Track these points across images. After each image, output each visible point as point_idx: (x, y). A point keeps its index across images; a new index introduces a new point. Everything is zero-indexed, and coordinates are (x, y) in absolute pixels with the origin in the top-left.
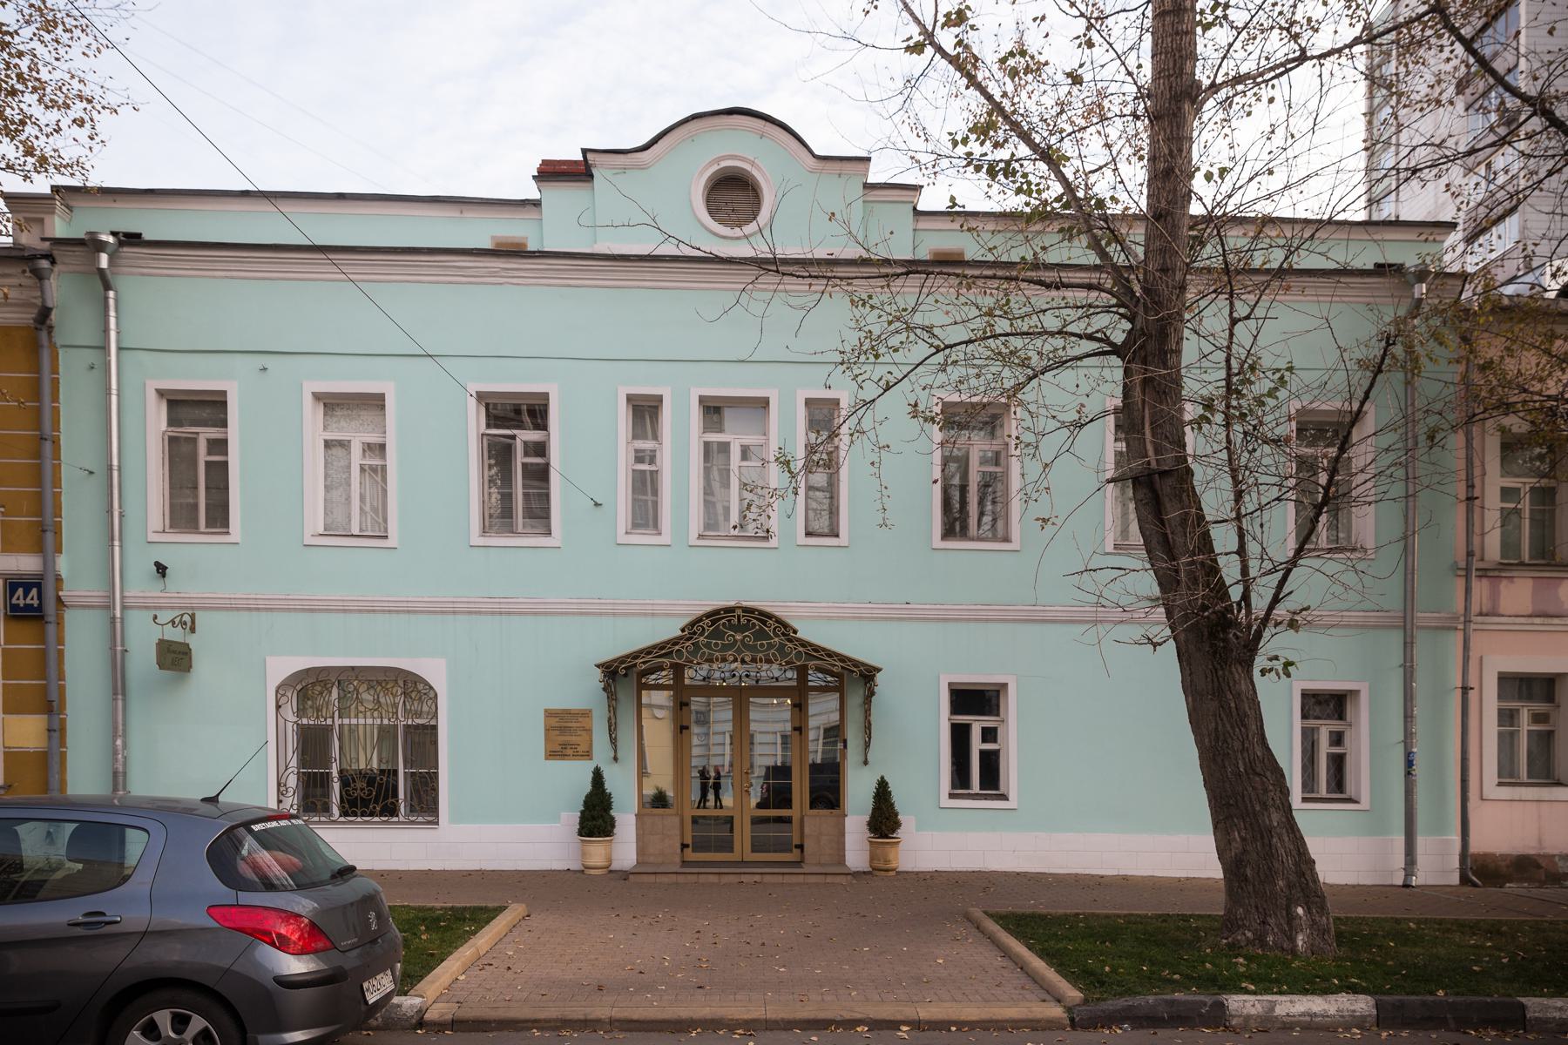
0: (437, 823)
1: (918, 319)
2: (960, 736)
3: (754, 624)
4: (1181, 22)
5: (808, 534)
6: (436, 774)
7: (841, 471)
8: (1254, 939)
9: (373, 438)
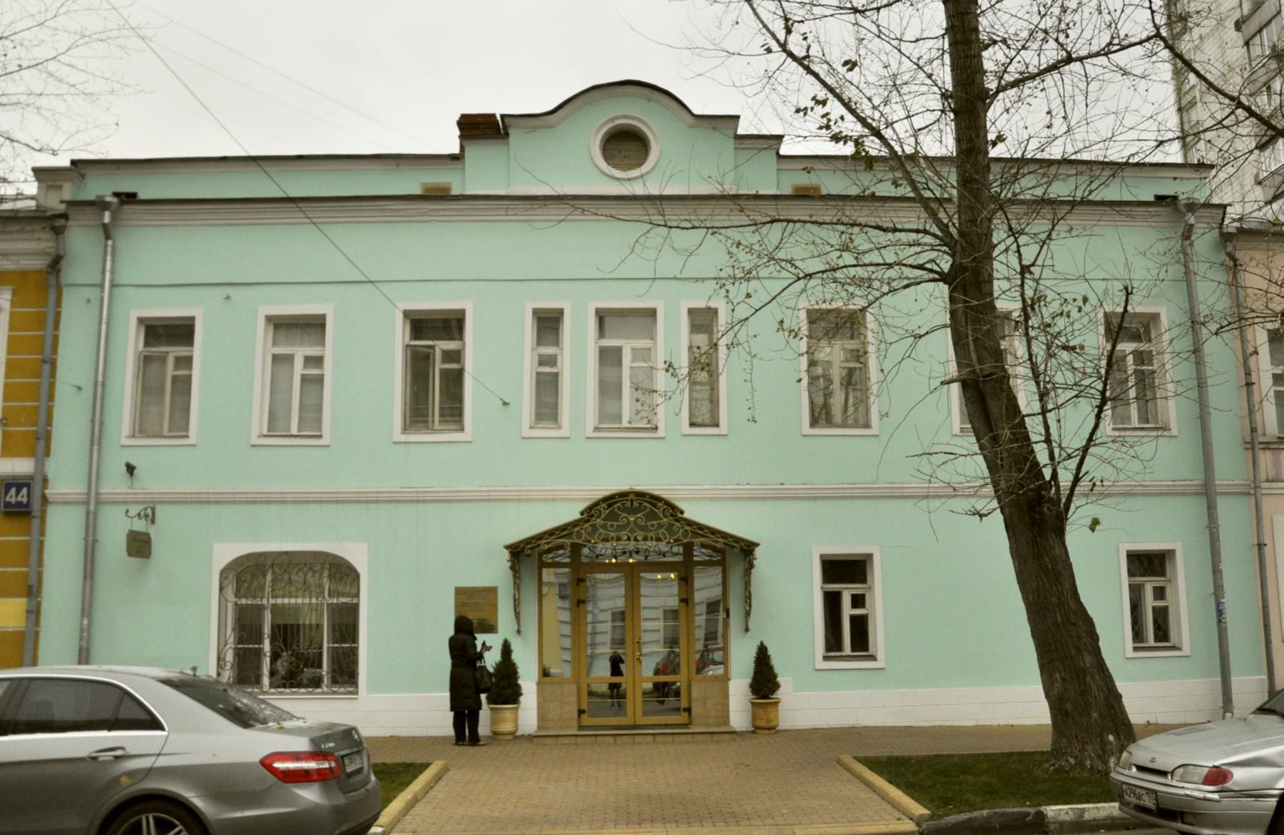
0: (357, 693)
1: (781, 255)
2: (832, 602)
3: (645, 507)
4: (970, 49)
5: (692, 424)
6: (357, 648)
7: (721, 377)
8: (1076, 764)
9: (313, 351)
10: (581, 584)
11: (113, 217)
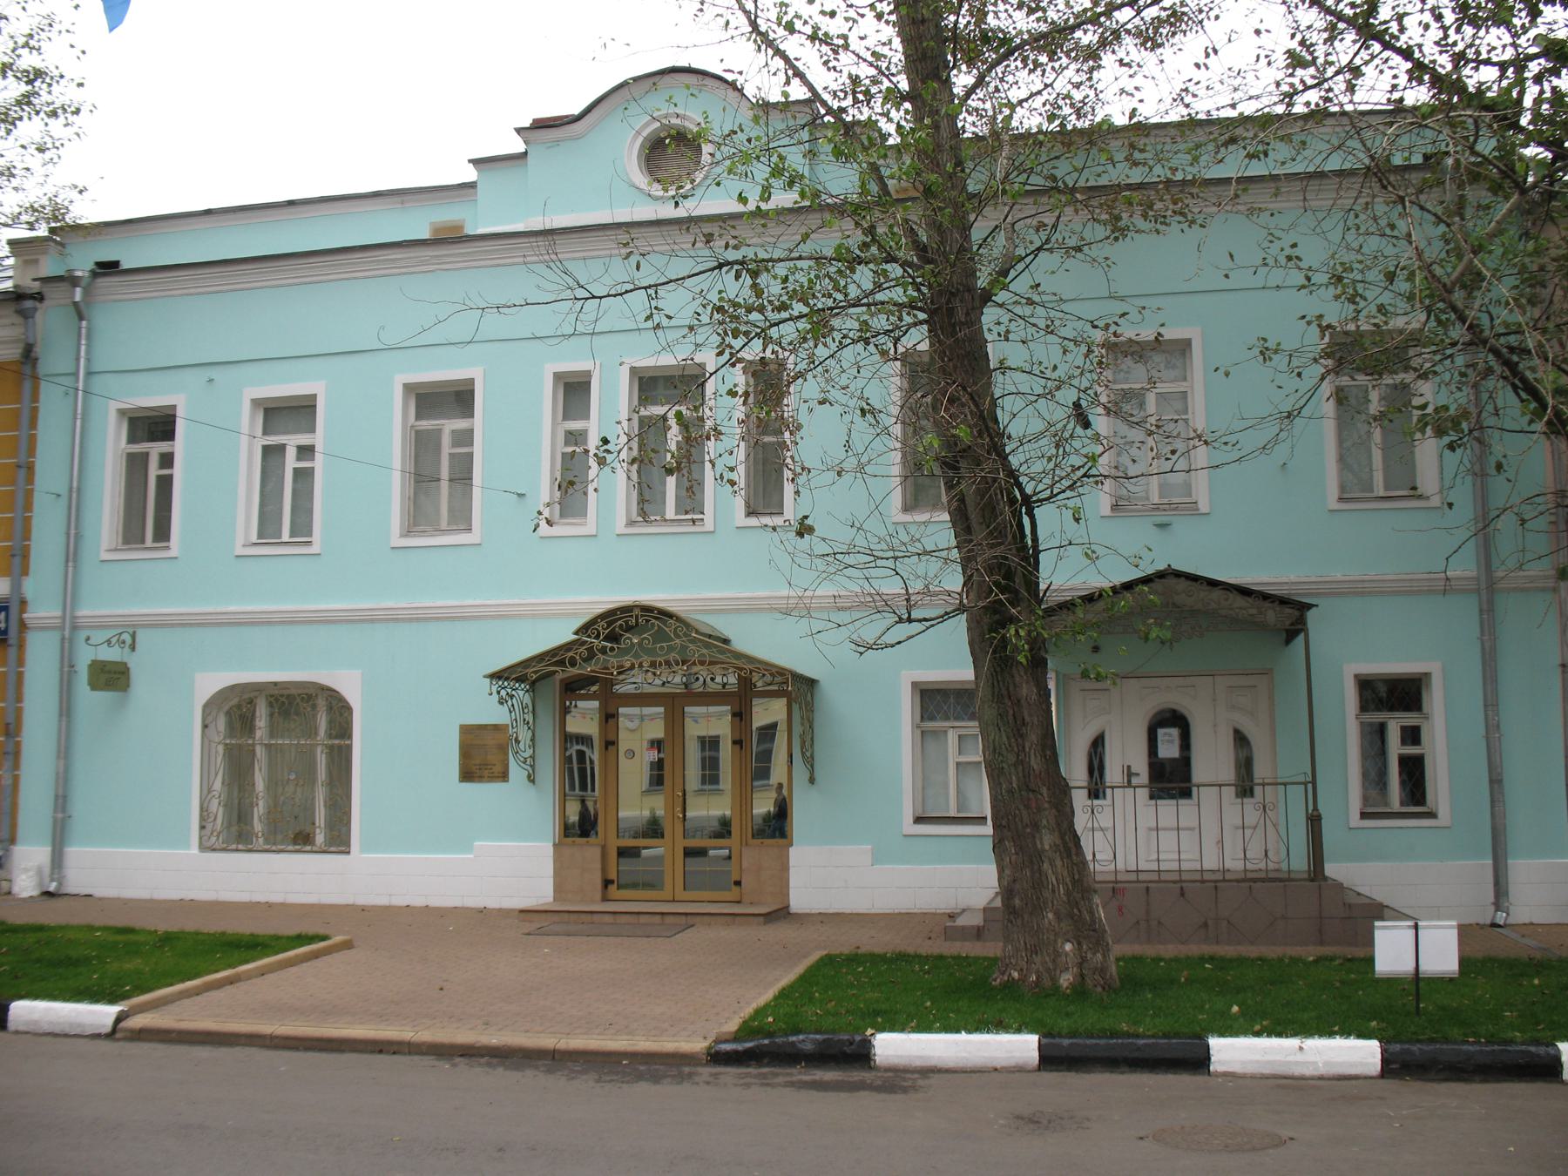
0: (349, 853)
3: (653, 624)
9: (304, 439)
10: (611, 721)
11: (87, 292)
